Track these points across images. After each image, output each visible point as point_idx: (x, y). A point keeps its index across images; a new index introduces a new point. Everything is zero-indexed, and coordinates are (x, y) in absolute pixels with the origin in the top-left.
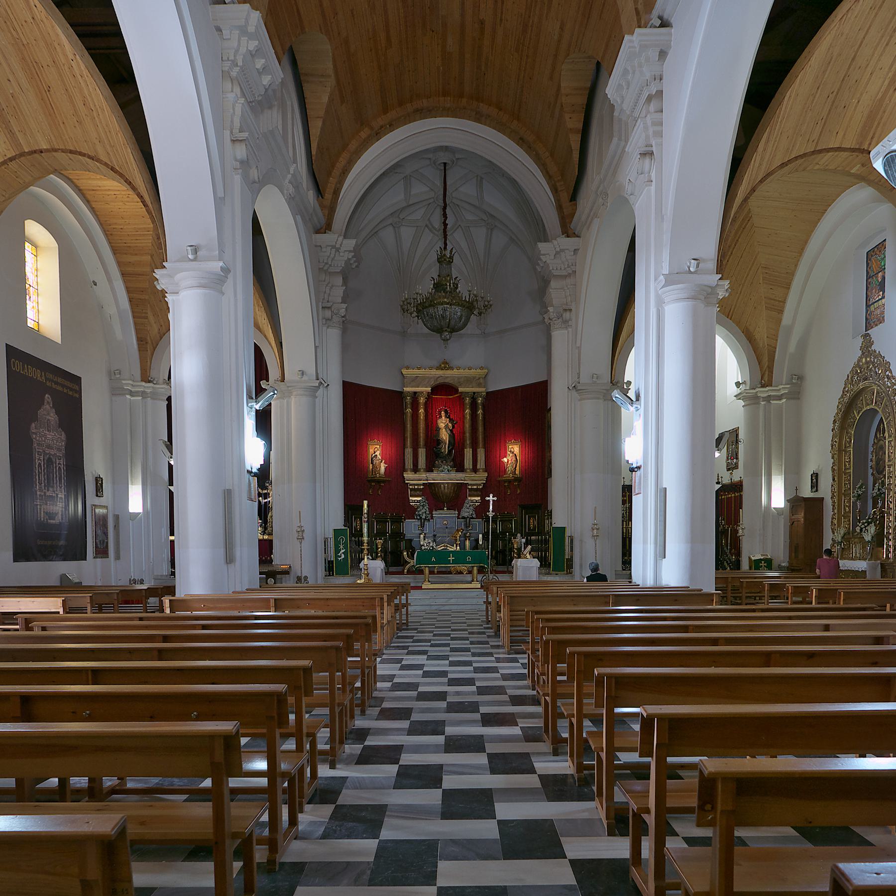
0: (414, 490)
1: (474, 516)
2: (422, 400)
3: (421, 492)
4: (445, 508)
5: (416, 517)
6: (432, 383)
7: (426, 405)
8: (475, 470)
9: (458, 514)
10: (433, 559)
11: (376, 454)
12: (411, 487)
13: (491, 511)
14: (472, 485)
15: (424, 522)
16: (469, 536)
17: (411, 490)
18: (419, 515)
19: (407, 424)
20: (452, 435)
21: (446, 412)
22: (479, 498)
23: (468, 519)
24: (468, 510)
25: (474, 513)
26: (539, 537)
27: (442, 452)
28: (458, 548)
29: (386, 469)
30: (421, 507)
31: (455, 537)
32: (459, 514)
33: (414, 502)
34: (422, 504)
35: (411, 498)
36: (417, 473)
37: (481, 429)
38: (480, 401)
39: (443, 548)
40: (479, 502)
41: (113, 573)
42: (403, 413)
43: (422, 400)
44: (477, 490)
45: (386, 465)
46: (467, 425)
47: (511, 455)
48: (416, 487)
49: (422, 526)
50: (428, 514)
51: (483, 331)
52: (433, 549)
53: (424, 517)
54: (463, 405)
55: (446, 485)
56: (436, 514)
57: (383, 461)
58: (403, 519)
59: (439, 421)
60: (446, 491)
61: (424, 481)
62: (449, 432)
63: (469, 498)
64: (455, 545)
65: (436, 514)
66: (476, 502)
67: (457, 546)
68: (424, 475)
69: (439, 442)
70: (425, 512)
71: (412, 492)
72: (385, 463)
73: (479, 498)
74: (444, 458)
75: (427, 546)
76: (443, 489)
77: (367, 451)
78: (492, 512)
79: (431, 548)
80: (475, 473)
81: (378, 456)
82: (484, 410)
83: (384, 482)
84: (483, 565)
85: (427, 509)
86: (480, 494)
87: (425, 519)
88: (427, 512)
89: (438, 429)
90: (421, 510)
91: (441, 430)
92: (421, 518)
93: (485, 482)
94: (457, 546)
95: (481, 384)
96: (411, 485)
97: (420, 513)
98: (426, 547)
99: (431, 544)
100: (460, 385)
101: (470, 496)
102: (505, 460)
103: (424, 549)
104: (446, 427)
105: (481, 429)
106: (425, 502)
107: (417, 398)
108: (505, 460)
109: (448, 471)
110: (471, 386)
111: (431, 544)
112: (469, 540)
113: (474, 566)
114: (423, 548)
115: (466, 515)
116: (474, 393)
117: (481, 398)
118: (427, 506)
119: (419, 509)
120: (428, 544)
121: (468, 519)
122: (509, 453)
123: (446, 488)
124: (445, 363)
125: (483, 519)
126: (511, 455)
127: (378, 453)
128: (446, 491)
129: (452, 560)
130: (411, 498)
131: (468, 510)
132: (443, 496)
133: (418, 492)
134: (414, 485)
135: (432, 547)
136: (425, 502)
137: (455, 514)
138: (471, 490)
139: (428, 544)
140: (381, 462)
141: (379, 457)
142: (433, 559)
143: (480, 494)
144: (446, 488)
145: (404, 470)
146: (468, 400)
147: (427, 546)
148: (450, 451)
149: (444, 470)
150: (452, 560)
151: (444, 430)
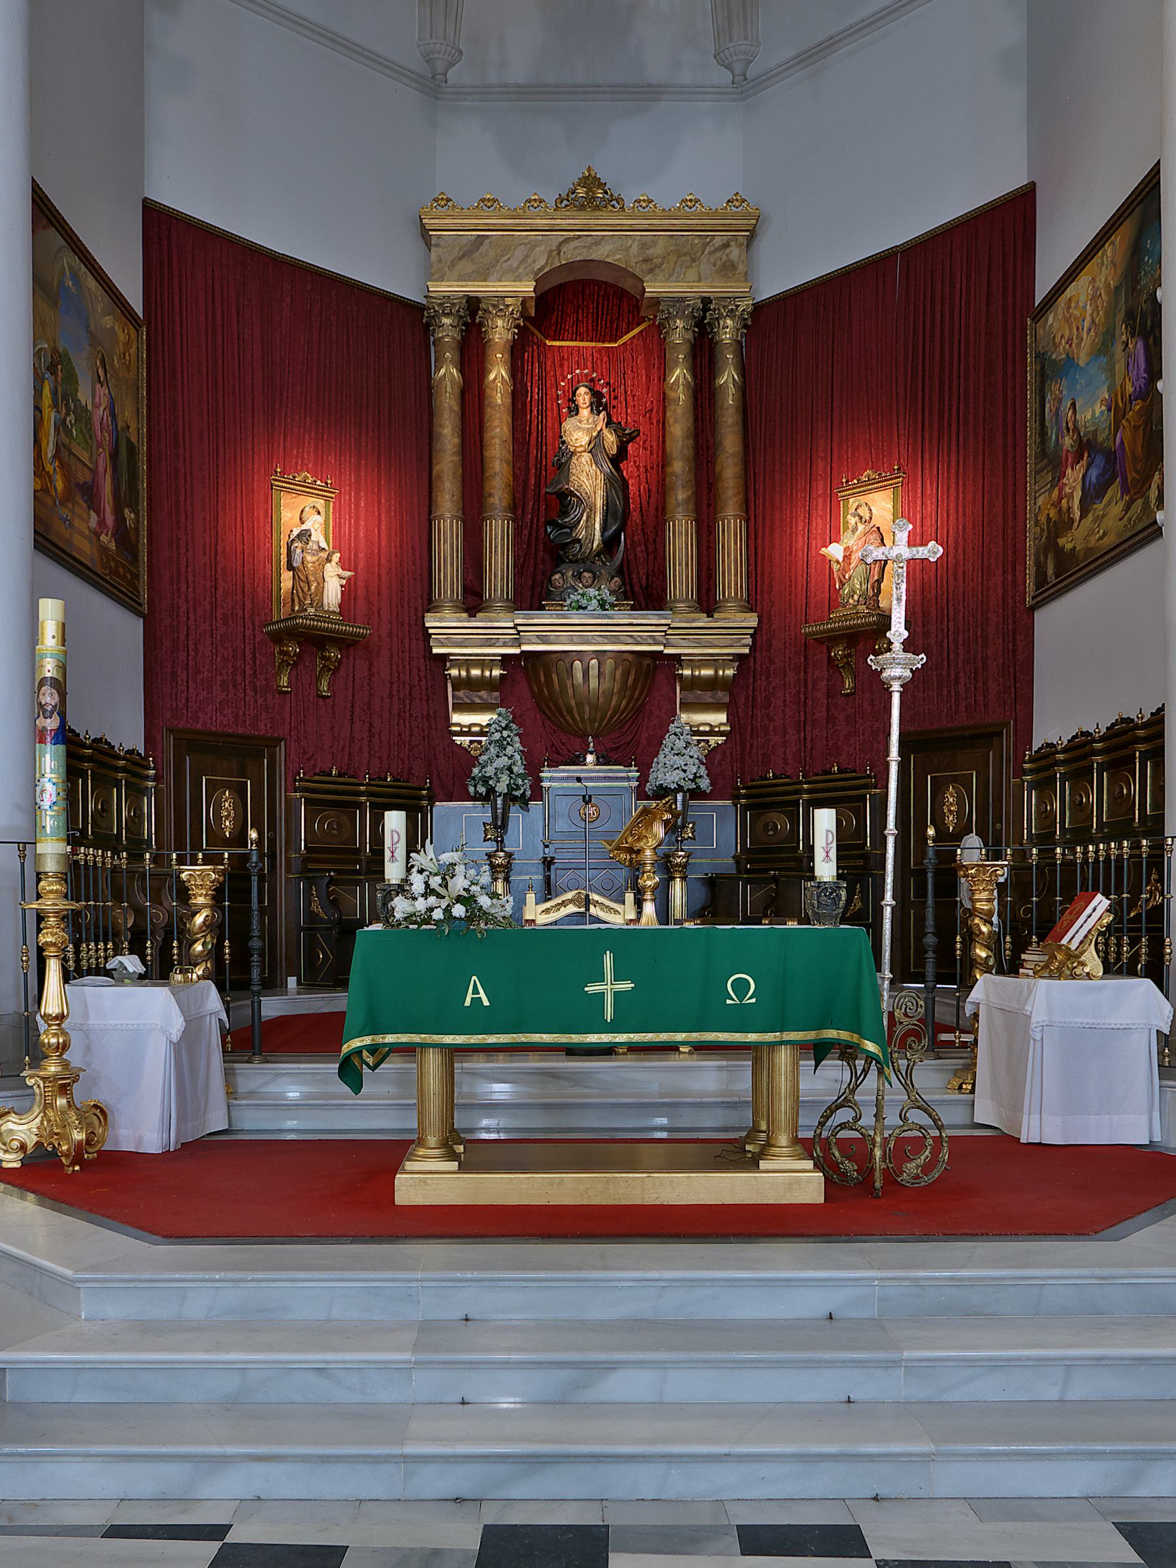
0: (469, 684)
1: (705, 784)
2: (500, 332)
3: (497, 694)
4: (590, 758)
5: (471, 789)
6: (540, 261)
7: (517, 351)
8: (707, 602)
9: (638, 779)
10: (477, 993)
11: (304, 527)
12: (454, 672)
13: (897, 646)
14: (695, 663)
15: (506, 810)
16: (685, 866)
17: (458, 684)
18: (485, 780)
19: (442, 426)
20: (617, 484)
21: (596, 395)
22: (722, 717)
23: (680, 797)
24: (680, 761)
25: (703, 771)
26: (1136, 846)
27: (579, 541)
28: (649, 908)
29: (348, 591)
30: (493, 750)
31: (630, 850)
32: (643, 779)
33: (469, 734)
34: (497, 736)
35: (456, 718)
36: (479, 615)
37: (730, 442)
38: (727, 331)
39: (572, 909)
40: (721, 734)
41: (678, 902)
42: (427, 390)
43: (500, 332)
44: (713, 683)
45: (348, 574)
46: (679, 428)
47: (861, 527)
48: (475, 672)
49: (499, 826)
50: (518, 775)
51: (739, 69)
52: (469, 919)
53: (502, 787)
54: (663, 357)
55: (594, 662)
56: (551, 779)
57: (336, 557)
58: (421, 798)
59: (569, 424)
60: (593, 683)
61: (505, 645)
62: (607, 467)
63: (684, 717)
64: (630, 897)
65: (554, 778)
66: (711, 733)
67: (639, 903)
68: (505, 621)
69: (564, 500)
70: (510, 769)
71: (461, 694)
72: (343, 564)
73: (722, 717)
74: (587, 564)
75: (429, 891)
76: (580, 679)
77: (270, 514)
78: (908, 646)
79: (459, 910)
80: (710, 615)
81: (318, 537)
82: (743, 370)
83: (346, 643)
84: (844, 1035)
85: (517, 757)
86: (727, 700)
87: (510, 798)
88: (518, 769)
89: (562, 462)
90: (491, 761)
91: (574, 460)
92: (491, 791)
93: (746, 651)
94: (639, 903)
95: (733, 267)
96: (458, 664)
97: (490, 771)
98: (421, 905)
99: (459, 884)
100: (651, 270)
101: (688, 706)
102: (835, 551)
103: (409, 918)
104: (596, 445)
105: (730, 442)
106: (506, 728)
107: (481, 324)
108: (835, 551)
109: (602, 605)
110: (692, 274)
111: (459, 884)
112: (683, 878)
113: (773, 1046)
114: (401, 907)
115: (671, 778)
116: (706, 301)
117: (732, 318)
118: (518, 745)
119: (484, 758)
120: (435, 882)
121: (680, 797)
122: (852, 520)
123: (594, 672)
124: (591, 182)
125: (736, 798)
126: (861, 527)
127: (315, 523)
128: (593, 683)
129: (617, 995)
130: (456, 718)
131: (680, 761)
132: (580, 705)
133: (483, 693)
134: (468, 663)
135: (467, 900)
136: (506, 728)
137: (628, 779)
138: (694, 683)
139: (435, 882)
140: (329, 560)
141: (318, 537)
142: (477, 993)
143: (727, 700)
144: (594, 672)
145: (430, 604)
146: (679, 333)
147: (429, 891)
148: (610, 544)
149: (584, 602)
150: (617, 995)
151: (586, 457)
